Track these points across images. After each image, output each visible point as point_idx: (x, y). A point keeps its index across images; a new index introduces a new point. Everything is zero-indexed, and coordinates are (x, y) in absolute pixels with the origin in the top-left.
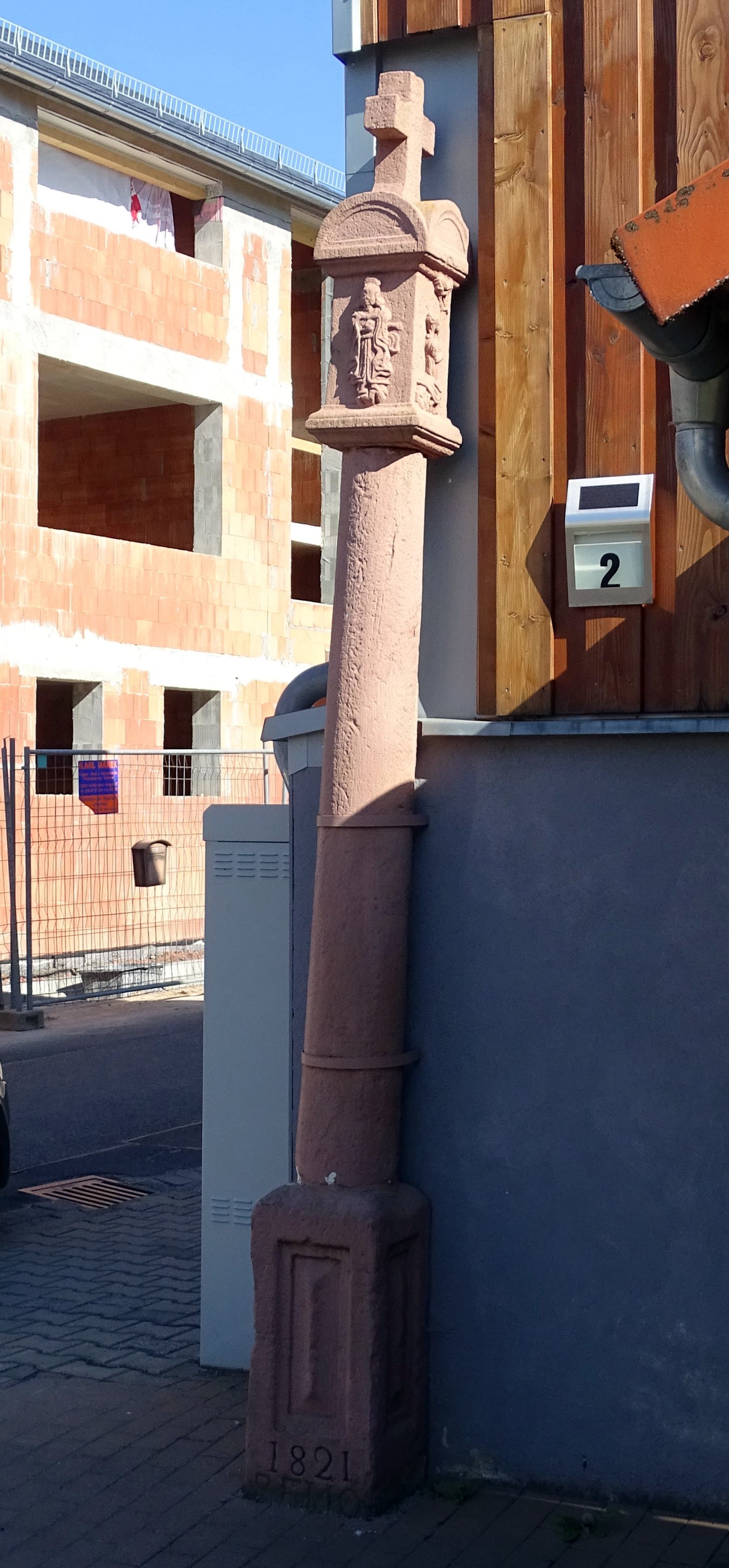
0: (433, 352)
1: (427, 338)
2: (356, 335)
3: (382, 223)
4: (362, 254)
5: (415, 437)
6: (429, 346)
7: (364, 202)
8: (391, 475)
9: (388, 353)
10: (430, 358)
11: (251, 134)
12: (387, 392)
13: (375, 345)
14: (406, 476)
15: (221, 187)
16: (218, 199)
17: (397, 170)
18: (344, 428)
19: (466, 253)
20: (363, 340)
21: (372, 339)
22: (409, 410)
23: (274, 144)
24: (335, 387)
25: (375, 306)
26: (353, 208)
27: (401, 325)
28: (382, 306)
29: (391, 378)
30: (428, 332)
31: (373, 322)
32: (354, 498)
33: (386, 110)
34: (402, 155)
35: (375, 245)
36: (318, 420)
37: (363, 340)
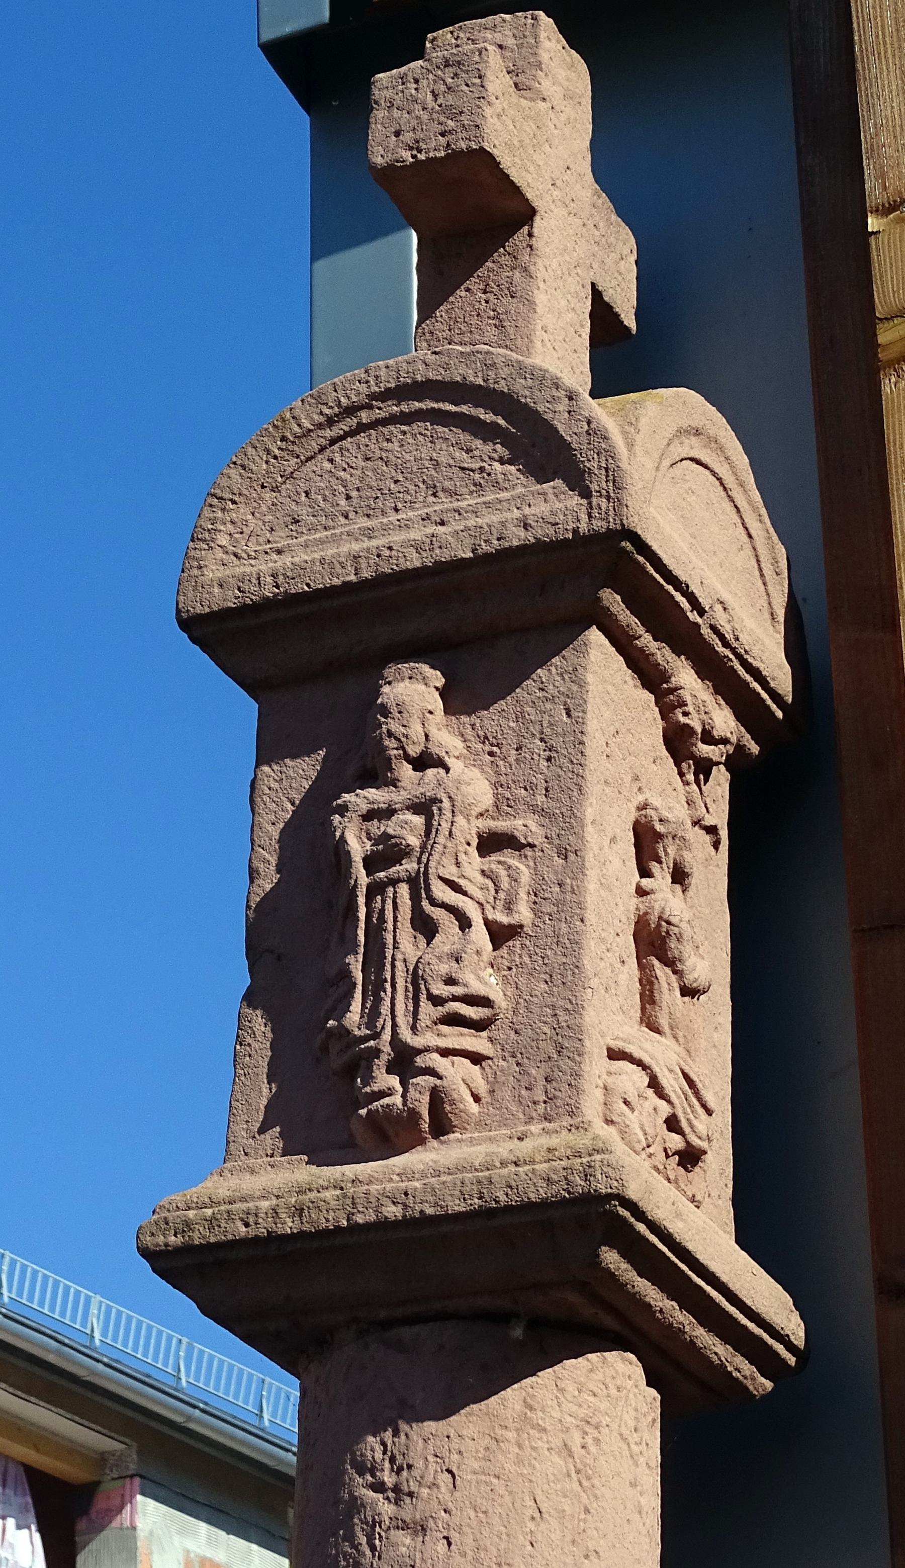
0: (673, 944)
1: (641, 892)
2: (349, 875)
3: (443, 459)
4: (366, 574)
5: (611, 1258)
6: (653, 919)
7: (373, 396)
8: (511, 1435)
9: (480, 935)
10: (661, 971)
11: (202, 1352)
12: (482, 1088)
13: (425, 904)
14: (576, 1440)
15: (135, 1457)
16: (128, 1480)
17: (500, 326)
18: (302, 1234)
19: (782, 628)
20: (375, 890)
21: (413, 881)
22: (582, 1141)
23: (251, 1376)
24: (265, 1092)
25: (423, 762)
26: (331, 422)
27: (533, 827)
28: (450, 761)
29: (500, 1032)
30: (645, 873)
31: (418, 821)
32: (350, 1537)
33: (450, 99)
34: (517, 274)
35: (416, 534)
36: (191, 1214)
37: (375, 890)
